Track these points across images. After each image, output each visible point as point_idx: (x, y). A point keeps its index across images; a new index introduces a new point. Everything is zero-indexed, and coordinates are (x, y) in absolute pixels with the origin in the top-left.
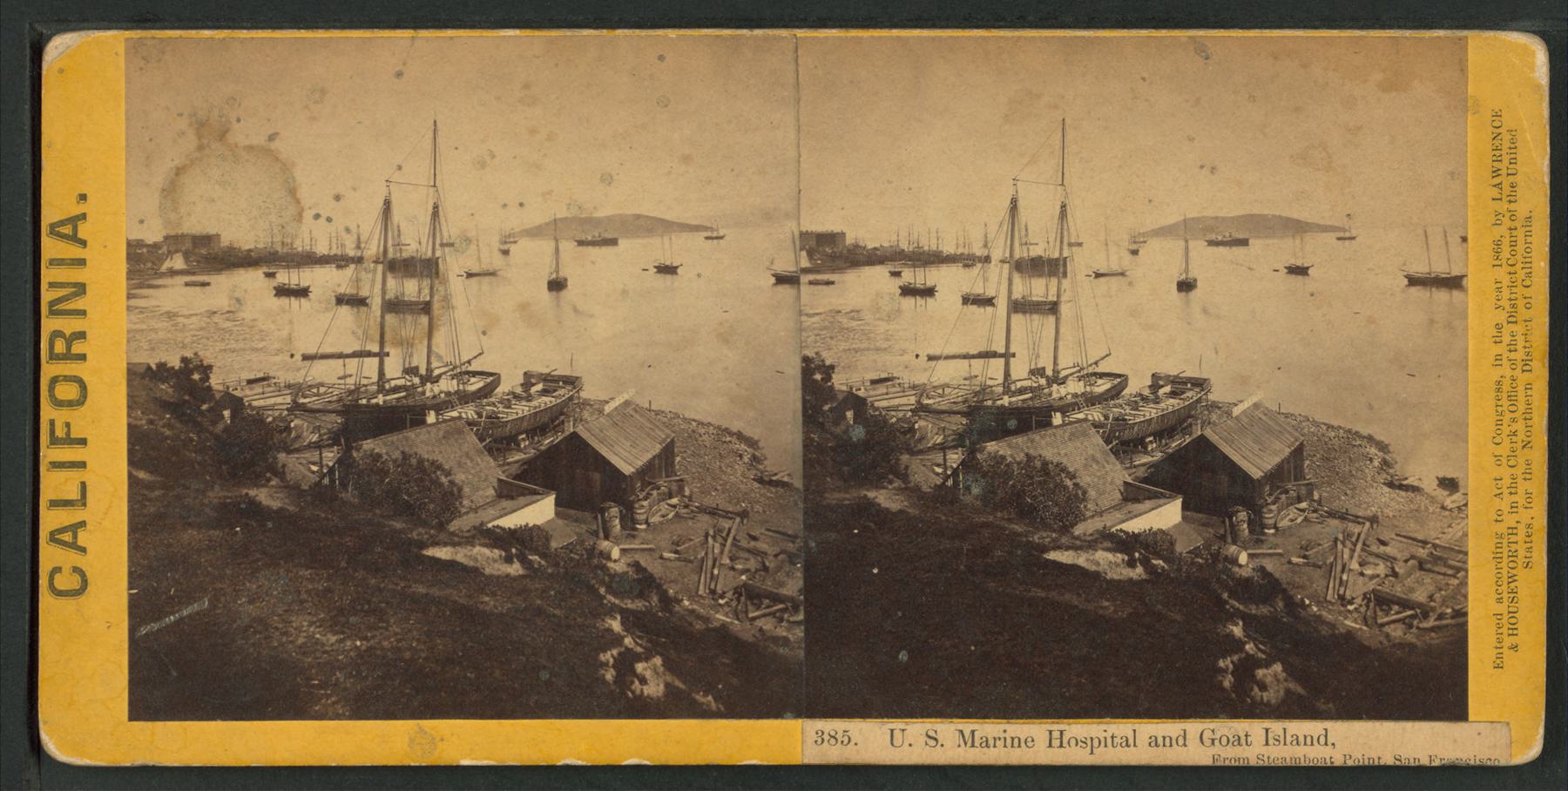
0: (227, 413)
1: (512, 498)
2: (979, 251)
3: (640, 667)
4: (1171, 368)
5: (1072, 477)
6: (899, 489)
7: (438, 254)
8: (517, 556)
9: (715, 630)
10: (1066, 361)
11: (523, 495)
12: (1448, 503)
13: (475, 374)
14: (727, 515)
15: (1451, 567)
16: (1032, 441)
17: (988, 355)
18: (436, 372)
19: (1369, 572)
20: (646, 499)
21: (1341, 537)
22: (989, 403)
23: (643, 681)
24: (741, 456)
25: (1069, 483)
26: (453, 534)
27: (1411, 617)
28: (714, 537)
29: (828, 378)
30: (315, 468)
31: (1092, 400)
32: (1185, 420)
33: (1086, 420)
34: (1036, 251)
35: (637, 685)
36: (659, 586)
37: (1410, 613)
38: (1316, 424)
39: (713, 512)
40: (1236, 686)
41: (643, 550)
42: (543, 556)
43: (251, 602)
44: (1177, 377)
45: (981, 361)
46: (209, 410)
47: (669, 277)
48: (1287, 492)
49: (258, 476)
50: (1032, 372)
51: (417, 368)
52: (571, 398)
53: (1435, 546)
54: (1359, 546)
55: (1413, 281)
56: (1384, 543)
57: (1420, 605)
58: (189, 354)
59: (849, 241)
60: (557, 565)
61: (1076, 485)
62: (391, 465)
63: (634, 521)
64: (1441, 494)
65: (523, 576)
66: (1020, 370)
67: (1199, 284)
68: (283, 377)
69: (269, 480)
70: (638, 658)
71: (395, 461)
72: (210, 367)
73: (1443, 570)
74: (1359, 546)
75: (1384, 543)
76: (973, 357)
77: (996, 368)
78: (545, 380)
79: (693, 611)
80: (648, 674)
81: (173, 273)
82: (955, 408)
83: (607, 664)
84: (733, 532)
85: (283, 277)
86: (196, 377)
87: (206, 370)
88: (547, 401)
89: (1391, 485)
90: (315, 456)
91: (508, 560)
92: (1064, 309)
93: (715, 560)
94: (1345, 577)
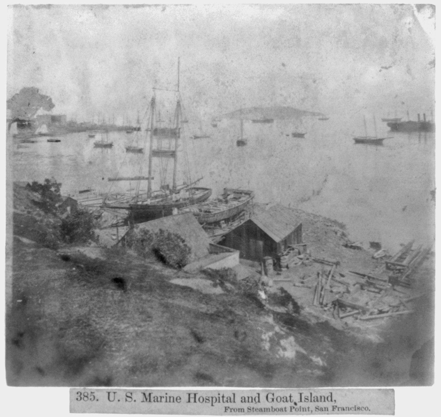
0: (69, 208)
1: (217, 253)
2: (134, 125)
3: (283, 342)
4: (234, 186)
5: (183, 241)
6: (95, 247)
7: (180, 126)
8: (220, 284)
9: (322, 323)
10: (179, 184)
11: (223, 252)
12: (376, 255)
13: (198, 189)
14: (329, 264)
15: (377, 288)
16: (162, 222)
17: (139, 178)
18: (178, 188)
19: (335, 290)
20: (286, 255)
21: (321, 273)
22: (140, 203)
23: (285, 349)
24: (336, 233)
25: (181, 244)
26: (186, 272)
27: (358, 313)
28: (322, 276)
29: (58, 190)
30: (114, 237)
31: (192, 202)
32: (240, 212)
33: (190, 212)
34: (162, 126)
35: (281, 352)
36: (293, 300)
37: (356, 311)
38: (308, 215)
39: (322, 262)
40: (271, 349)
41: (286, 281)
42: (233, 283)
43: (80, 307)
44: (237, 190)
45: (137, 181)
46: (60, 206)
47: (300, 139)
48: (293, 249)
49: (85, 241)
50: (163, 187)
51: (168, 186)
52: (248, 202)
53: (369, 277)
54: (330, 277)
55: (358, 141)
56: (342, 276)
57: (362, 308)
58: (49, 177)
59: (68, 119)
60: (240, 288)
61: (185, 245)
62: (154, 236)
63: (280, 266)
64: (372, 250)
65: (221, 295)
66: (155, 187)
67: (248, 143)
68: (98, 189)
69: (90, 244)
70: (281, 337)
71: (156, 234)
72: (60, 184)
73: (373, 290)
74: (330, 277)
75: (342, 276)
76: (132, 179)
77: (144, 184)
78: (235, 192)
79: (310, 314)
80: (287, 346)
81: (41, 135)
82: (123, 206)
83: (266, 340)
84: (332, 273)
85: (98, 137)
86: (53, 189)
87: (58, 186)
88: (235, 203)
89: (346, 246)
90: (114, 231)
91: (215, 285)
92: (179, 154)
93: (322, 288)
94: (323, 293)
